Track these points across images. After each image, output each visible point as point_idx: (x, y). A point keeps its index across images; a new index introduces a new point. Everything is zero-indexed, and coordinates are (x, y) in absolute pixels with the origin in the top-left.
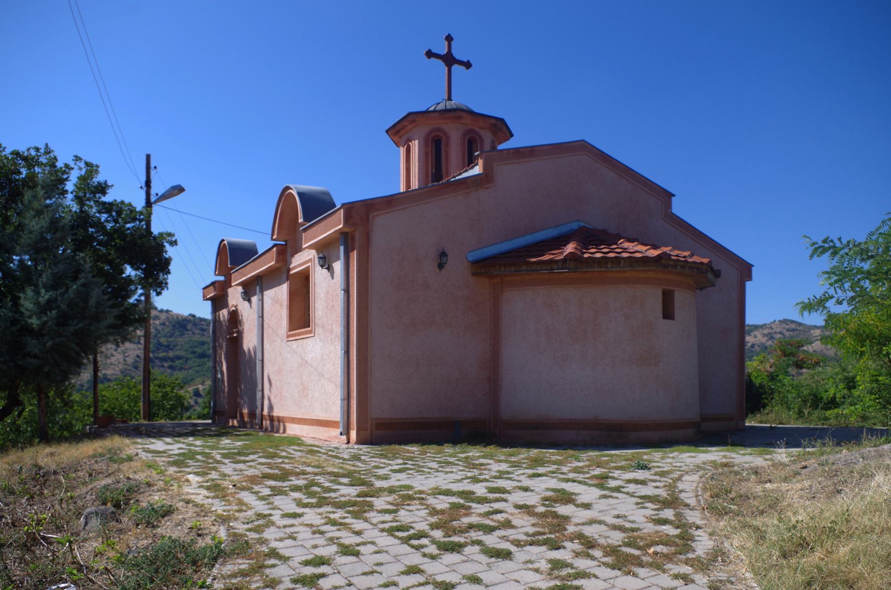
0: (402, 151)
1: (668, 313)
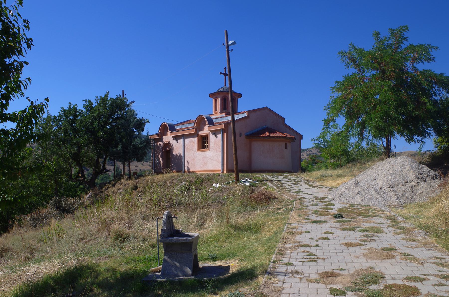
0: (214, 100)
1: (286, 148)
